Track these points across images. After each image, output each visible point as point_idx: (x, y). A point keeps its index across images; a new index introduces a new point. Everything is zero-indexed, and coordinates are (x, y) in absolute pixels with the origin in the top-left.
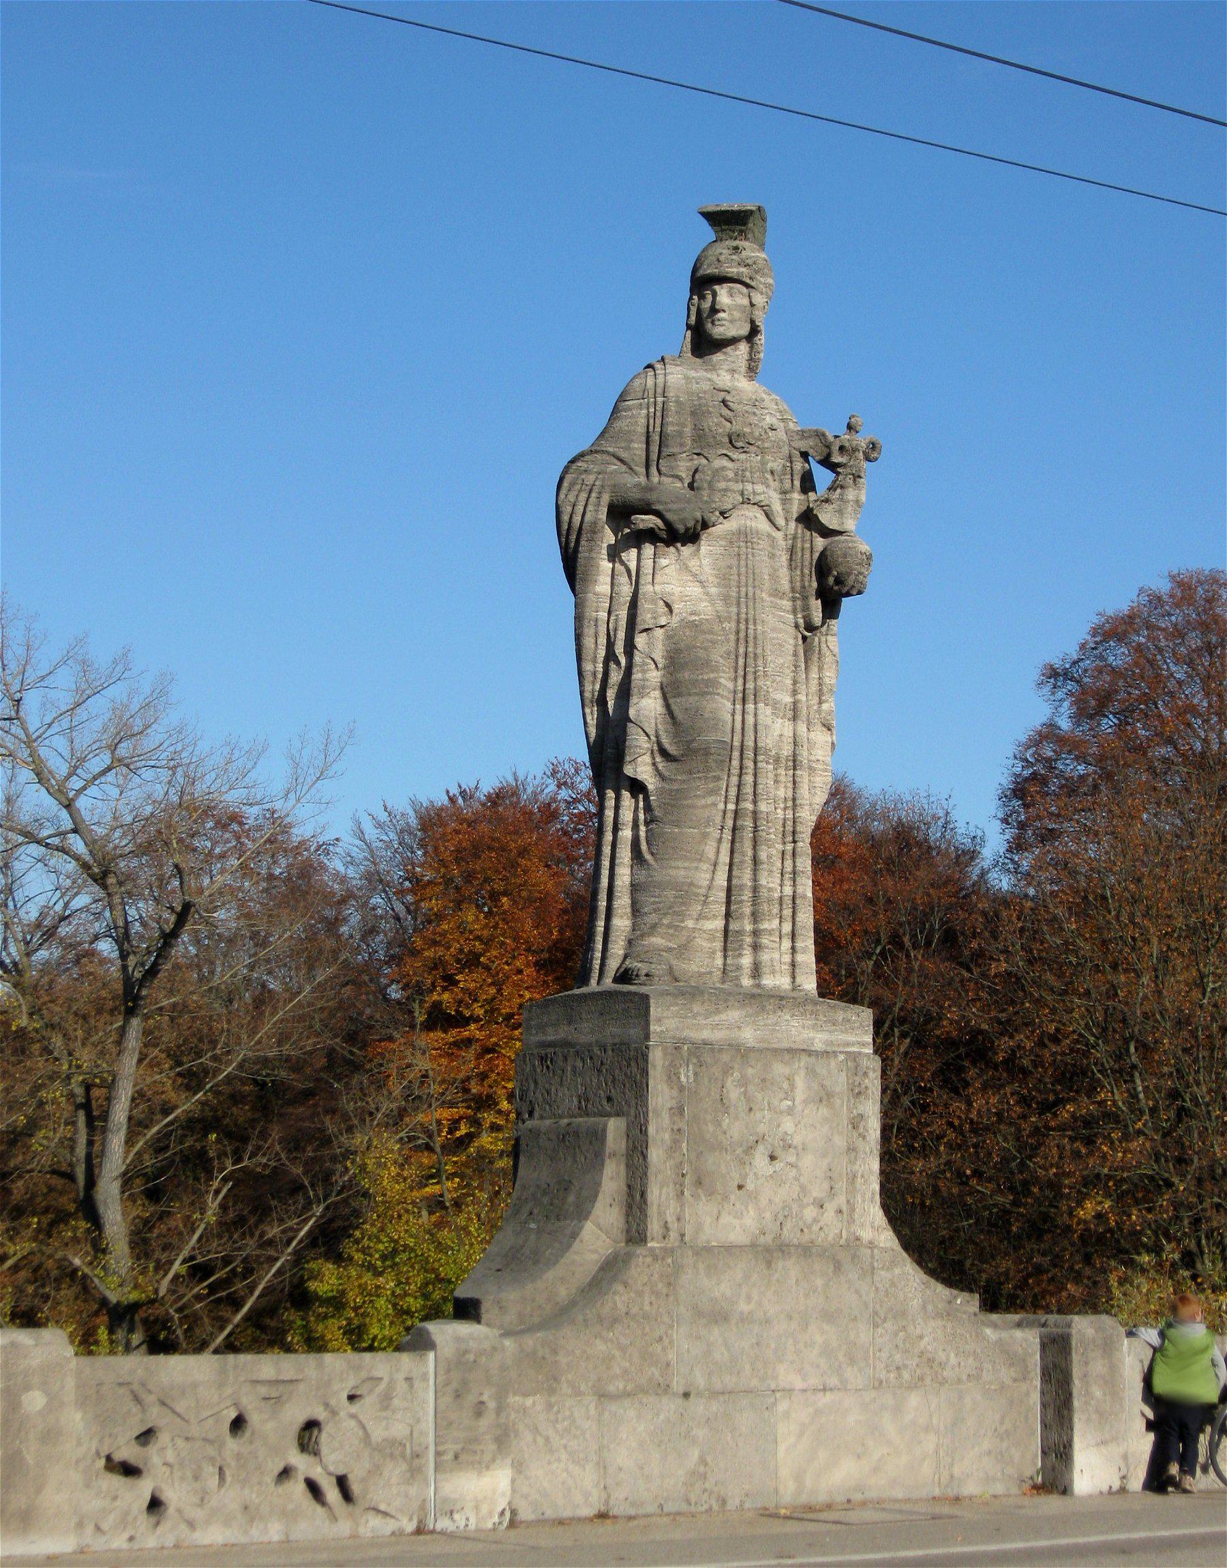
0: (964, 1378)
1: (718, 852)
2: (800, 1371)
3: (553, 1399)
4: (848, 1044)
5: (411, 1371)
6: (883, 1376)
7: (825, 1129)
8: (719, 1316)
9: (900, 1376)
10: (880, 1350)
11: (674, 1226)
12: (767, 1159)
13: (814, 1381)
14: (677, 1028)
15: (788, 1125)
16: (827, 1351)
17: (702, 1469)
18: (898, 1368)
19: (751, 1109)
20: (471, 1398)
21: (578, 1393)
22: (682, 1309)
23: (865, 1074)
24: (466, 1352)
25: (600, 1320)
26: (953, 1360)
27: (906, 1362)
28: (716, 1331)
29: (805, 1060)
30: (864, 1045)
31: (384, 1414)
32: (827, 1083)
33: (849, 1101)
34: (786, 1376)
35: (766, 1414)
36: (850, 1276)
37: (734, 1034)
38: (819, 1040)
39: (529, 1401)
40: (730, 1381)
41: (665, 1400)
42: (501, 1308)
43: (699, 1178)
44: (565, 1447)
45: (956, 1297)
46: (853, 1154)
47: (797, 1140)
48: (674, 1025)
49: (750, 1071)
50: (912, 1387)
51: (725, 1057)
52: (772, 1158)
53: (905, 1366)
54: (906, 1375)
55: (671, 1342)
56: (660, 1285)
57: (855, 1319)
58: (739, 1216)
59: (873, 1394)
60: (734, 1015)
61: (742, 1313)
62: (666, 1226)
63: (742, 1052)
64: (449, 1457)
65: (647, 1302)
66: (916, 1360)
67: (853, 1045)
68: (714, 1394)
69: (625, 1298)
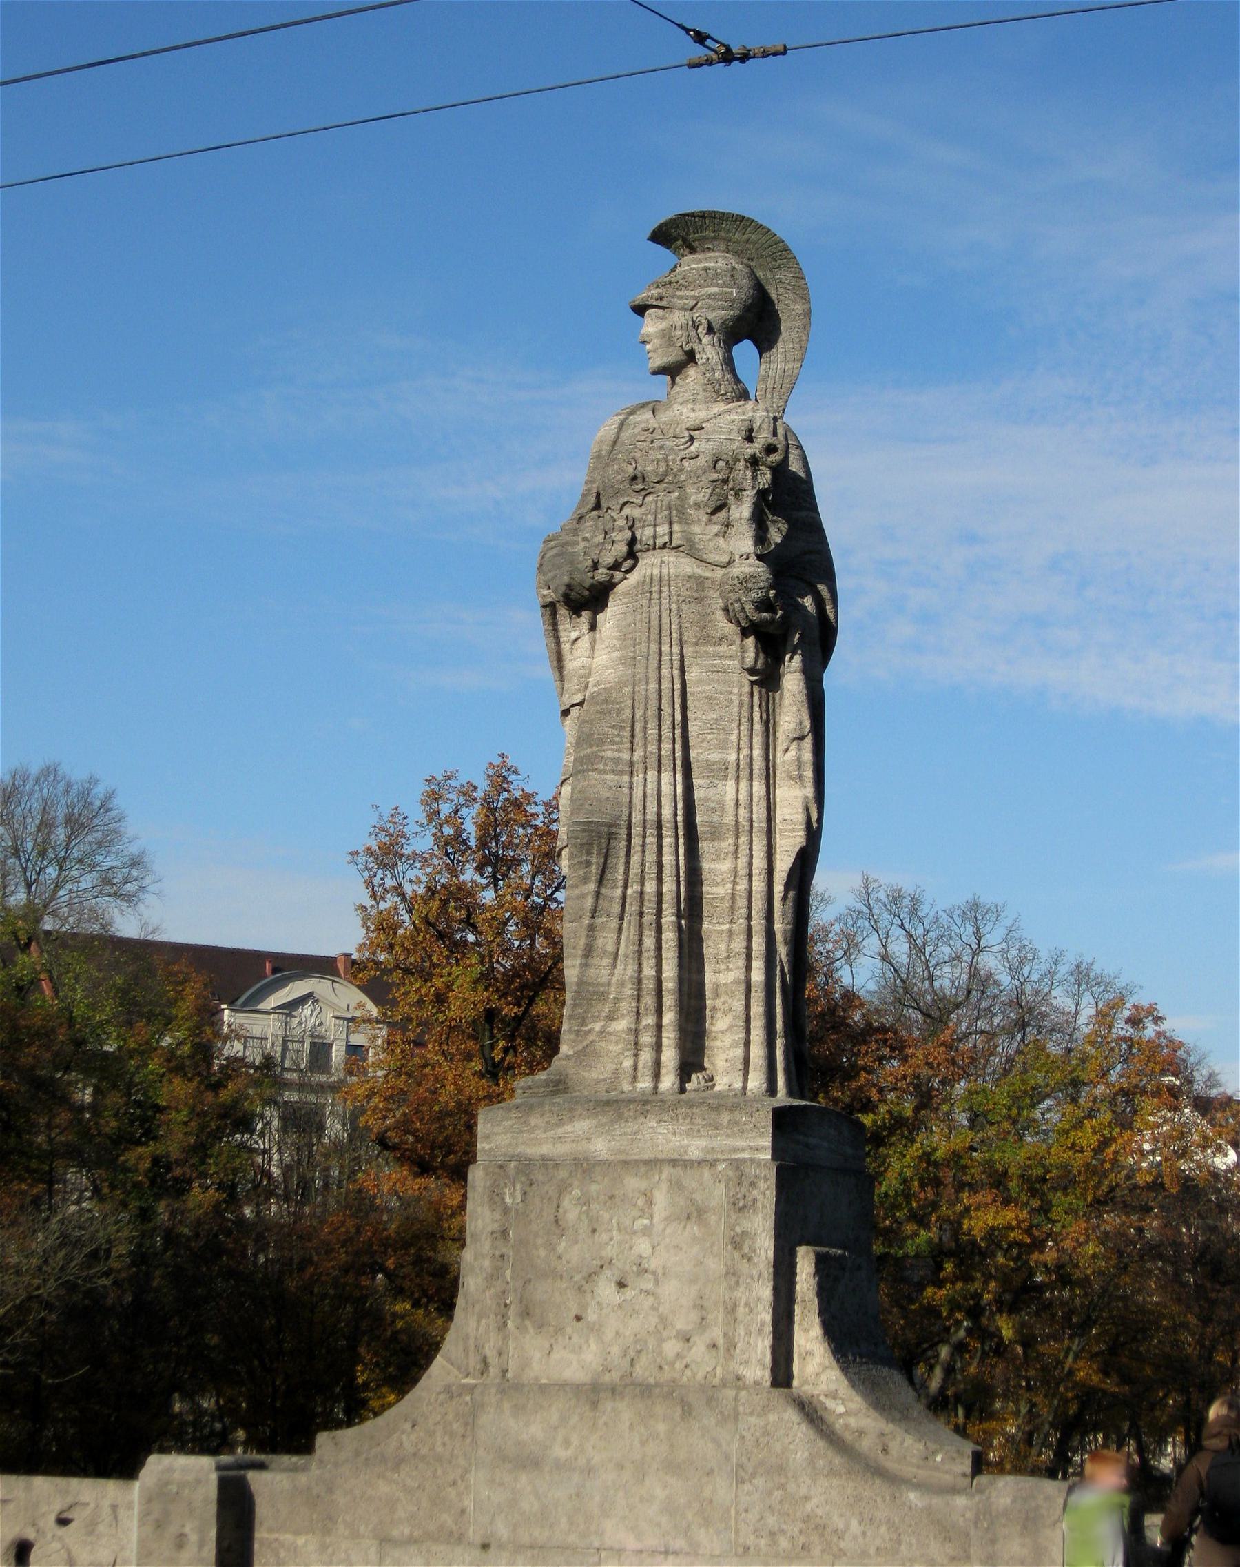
0: (872, 1551)
1: (618, 944)
3: (328, 1540)
4: (736, 1150)
6: (751, 1540)
7: (696, 1249)
8: (529, 1461)
9: (774, 1543)
10: (746, 1511)
11: (494, 1360)
12: (614, 1288)
13: (652, 1541)
14: (510, 1144)
15: (643, 1246)
16: (670, 1508)
18: (772, 1534)
19: (594, 1231)
20: (173, 1530)
21: (355, 1535)
22: (481, 1452)
23: (753, 1184)
24: (167, 1483)
25: (383, 1459)
27: (785, 1527)
28: (524, 1478)
29: (667, 1171)
30: (763, 1148)
31: (89, 1539)
32: (698, 1197)
33: (729, 1216)
36: (705, 1421)
37: (581, 1147)
38: (695, 1147)
39: (301, 1541)
40: (540, 1535)
42: (336, 1444)
43: (527, 1307)
45: (934, 1453)
46: (734, 1279)
47: (654, 1264)
48: (507, 1141)
49: (594, 1187)
51: (563, 1174)
52: (621, 1285)
53: (783, 1531)
54: (784, 1543)
55: (467, 1487)
56: (455, 1426)
57: (710, 1473)
58: (578, 1350)
60: (582, 1126)
61: (557, 1460)
62: (485, 1360)
63: (584, 1166)
65: (439, 1443)
66: (800, 1525)
67: (743, 1150)
69: (413, 1437)
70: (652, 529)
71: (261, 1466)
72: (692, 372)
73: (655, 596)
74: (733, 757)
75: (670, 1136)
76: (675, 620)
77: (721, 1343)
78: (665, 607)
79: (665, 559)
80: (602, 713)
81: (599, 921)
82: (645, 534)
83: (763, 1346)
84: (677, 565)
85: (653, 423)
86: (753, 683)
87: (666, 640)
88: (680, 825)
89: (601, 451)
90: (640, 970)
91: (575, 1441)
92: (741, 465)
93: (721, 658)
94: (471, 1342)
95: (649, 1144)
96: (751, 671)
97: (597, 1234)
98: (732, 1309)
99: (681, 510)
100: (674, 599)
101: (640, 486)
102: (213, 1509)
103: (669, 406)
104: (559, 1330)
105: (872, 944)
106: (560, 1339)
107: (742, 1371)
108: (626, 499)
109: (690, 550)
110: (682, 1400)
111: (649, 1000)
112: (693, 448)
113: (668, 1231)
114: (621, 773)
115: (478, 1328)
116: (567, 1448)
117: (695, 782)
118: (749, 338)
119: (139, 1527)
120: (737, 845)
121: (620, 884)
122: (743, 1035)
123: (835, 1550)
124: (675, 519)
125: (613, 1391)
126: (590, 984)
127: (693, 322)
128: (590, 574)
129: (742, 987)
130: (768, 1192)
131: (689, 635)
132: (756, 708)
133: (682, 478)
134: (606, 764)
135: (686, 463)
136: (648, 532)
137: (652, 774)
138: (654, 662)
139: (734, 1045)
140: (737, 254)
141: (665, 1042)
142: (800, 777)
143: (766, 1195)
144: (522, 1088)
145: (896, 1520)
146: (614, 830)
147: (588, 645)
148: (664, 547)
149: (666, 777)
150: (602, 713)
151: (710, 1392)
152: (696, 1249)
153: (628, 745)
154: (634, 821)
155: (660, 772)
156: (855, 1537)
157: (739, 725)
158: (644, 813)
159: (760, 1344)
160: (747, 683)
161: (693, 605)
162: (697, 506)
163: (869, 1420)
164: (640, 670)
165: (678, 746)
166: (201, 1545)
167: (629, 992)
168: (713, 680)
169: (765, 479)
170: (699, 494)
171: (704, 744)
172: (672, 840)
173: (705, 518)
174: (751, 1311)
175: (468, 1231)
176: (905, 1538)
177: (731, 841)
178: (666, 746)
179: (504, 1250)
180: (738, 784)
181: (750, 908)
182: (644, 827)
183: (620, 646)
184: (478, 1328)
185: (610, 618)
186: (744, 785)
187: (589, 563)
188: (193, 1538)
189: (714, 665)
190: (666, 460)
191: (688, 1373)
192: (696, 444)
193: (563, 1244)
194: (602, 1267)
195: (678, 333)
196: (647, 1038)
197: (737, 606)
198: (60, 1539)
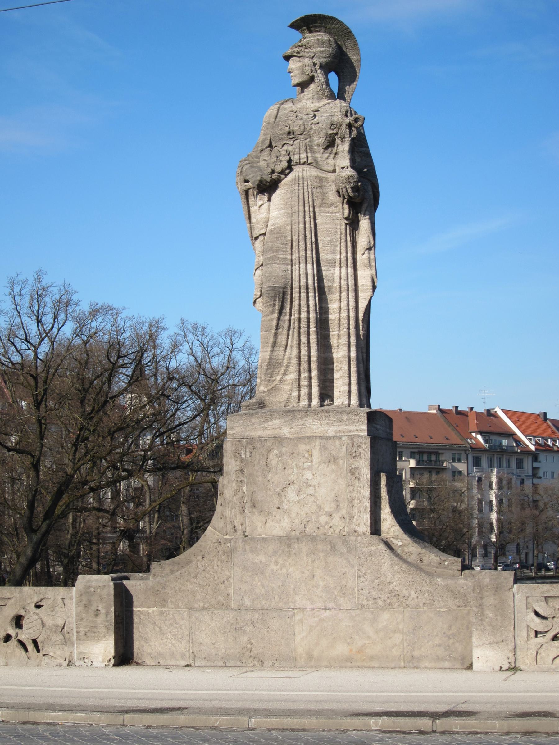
0: (421, 605)
2: (310, 599)
4: (350, 431)
5: (64, 595)
6: (365, 602)
7: (333, 476)
11: (239, 527)
13: (319, 605)
14: (243, 431)
15: (308, 475)
17: (249, 646)
18: (375, 599)
19: (285, 468)
20: (93, 608)
24: (89, 587)
26: (413, 595)
29: (318, 442)
30: (363, 430)
32: (333, 452)
34: (300, 601)
35: (289, 620)
37: (277, 432)
38: (331, 431)
39: (151, 610)
40: (265, 603)
41: (227, 612)
43: (254, 503)
44: (170, 632)
45: (444, 561)
46: (352, 488)
47: (314, 482)
49: (284, 450)
50: (383, 609)
51: (269, 444)
54: (380, 603)
59: (358, 612)
60: (277, 422)
63: (279, 440)
64: (82, 634)
65: (216, 565)
67: (354, 431)
68: (256, 610)
69: (203, 563)
70: (298, 155)
71: (127, 578)
72: (312, 86)
73: (301, 185)
74: (338, 257)
75: (319, 425)
76: (310, 196)
77: (346, 516)
78: (306, 190)
79: (305, 169)
80: (278, 238)
81: (279, 330)
82: (296, 158)
83: (366, 517)
84: (310, 172)
85: (295, 109)
86: (346, 224)
87: (307, 205)
88: (316, 287)
89: (269, 120)
90: (300, 352)
91: (280, 561)
92: (344, 127)
93: (332, 213)
94: (228, 520)
95: (309, 429)
96: (346, 219)
97: (286, 470)
98: (351, 501)
99: (311, 147)
100: (310, 186)
101: (292, 136)
102: (112, 598)
103: (300, 101)
104: (269, 513)
105: (185, 348)
106: (270, 517)
107: (356, 528)
108: (285, 142)
109: (316, 165)
110: (331, 542)
111: (304, 366)
112: (315, 120)
113: (320, 468)
114: (287, 265)
115: (231, 514)
116: (277, 565)
117: (323, 268)
118: (334, 71)
119: (76, 607)
120: (340, 296)
121: (288, 314)
122: (348, 380)
123: (404, 605)
124: (309, 151)
125: (298, 539)
126: (275, 359)
127: (314, 63)
128: (270, 176)
129: (347, 359)
130: (367, 449)
131: (317, 203)
132: (348, 235)
133: (312, 132)
134: (280, 261)
135: (313, 126)
136: (297, 157)
137: (303, 265)
138: (301, 215)
139: (344, 385)
140: (329, 33)
141: (313, 384)
142: (370, 266)
143: (365, 450)
144: (245, 406)
145: (432, 591)
146: (285, 290)
147: (267, 207)
148: (304, 163)
149: (309, 266)
150: (278, 238)
151: (344, 538)
152: (333, 476)
153: (290, 252)
154: (294, 286)
155: (306, 264)
156: (413, 599)
157: (341, 243)
158: (300, 283)
159: (365, 516)
160: (344, 224)
161: (318, 190)
162: (318, 145)
163: (414, 548)
164: (295, 218)
165: (314, 252)
166: (107, 614)
167: (295, 362)
168: (328, 223)
169: (354, 133)
170: (319, 140)
171: (325, 251)
172: (313, 294)
173: (322, 151)
174: (360, 502)
175: (224, 470)
176: (436, 598)
177: (338, 294)
178: (309, 252)
179: (242, 479)
180: (340, 269)
181: (349, 324)
182: (300, 288)
183: (284, 208)
184: (231, 514)
185: (277, 196)
186: (344, 270)
187: (270, 170)
188: (103, 611)
189: (328, 216)
190: (304, 125)
191: (332, 530)
192: (317, 118)
193: (270, 475)
194: (289, 484)
195: (307, 68)
196: (304, 383)
197: (344, 190)
198: (37, 614)
